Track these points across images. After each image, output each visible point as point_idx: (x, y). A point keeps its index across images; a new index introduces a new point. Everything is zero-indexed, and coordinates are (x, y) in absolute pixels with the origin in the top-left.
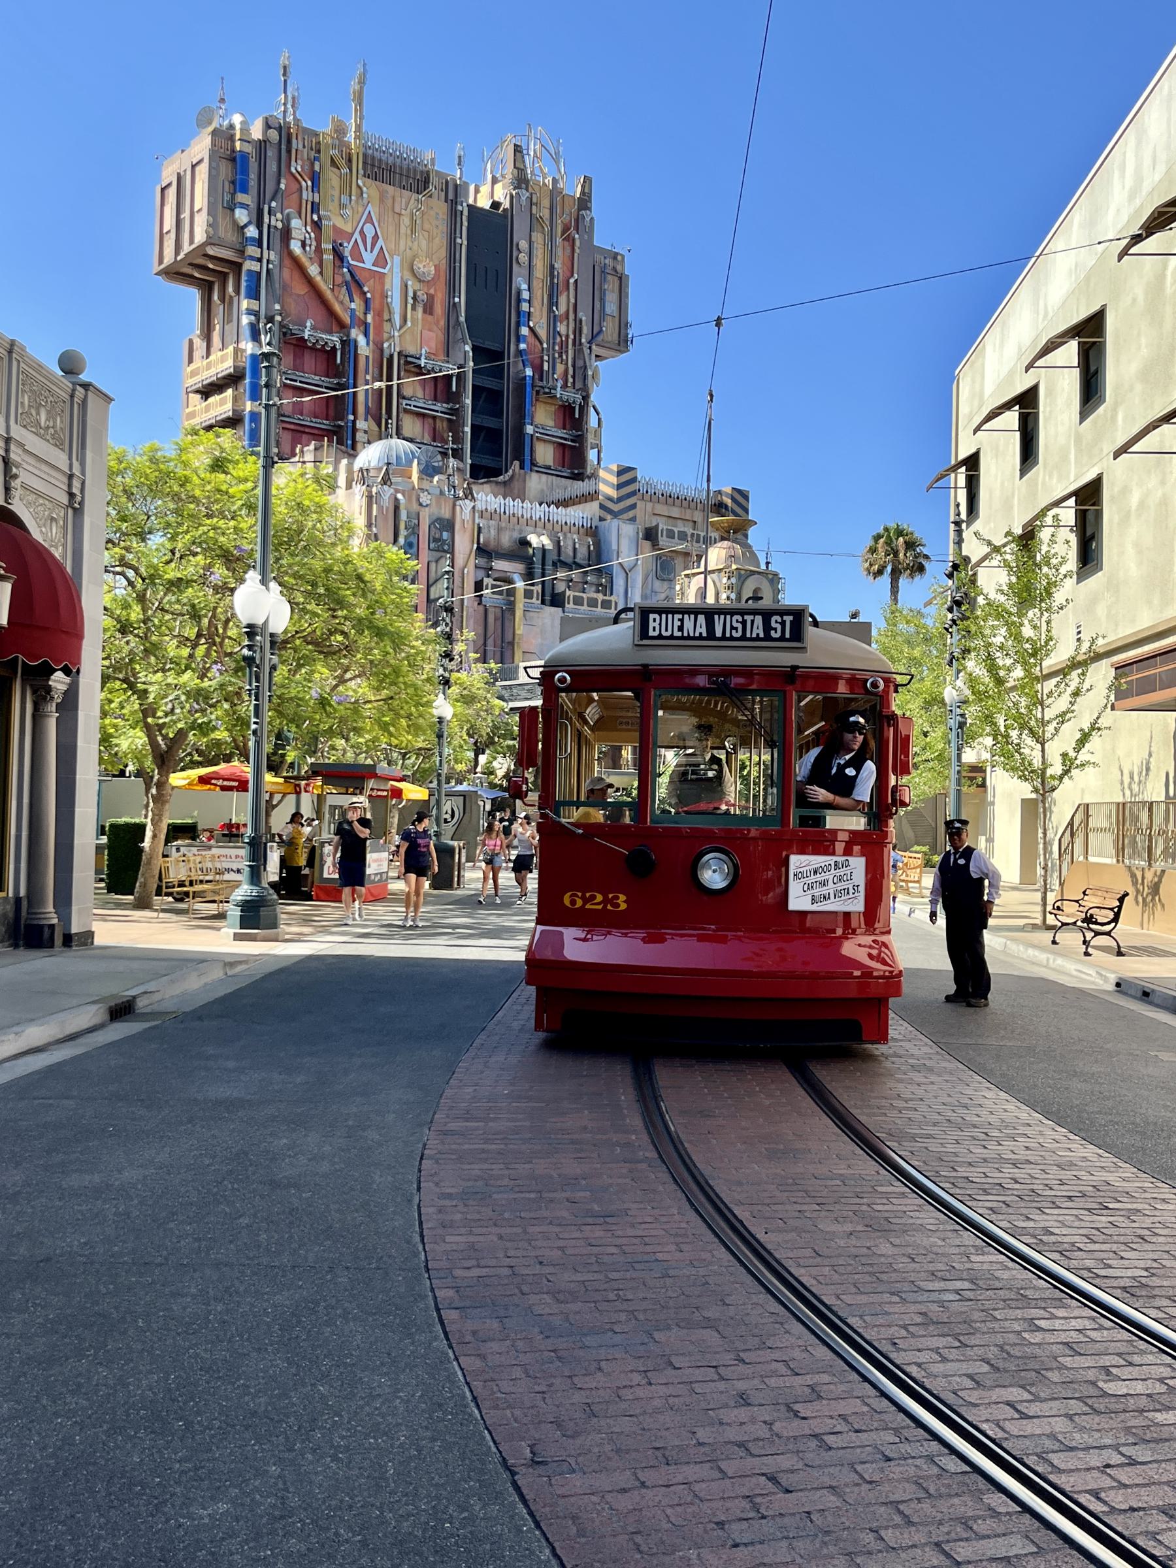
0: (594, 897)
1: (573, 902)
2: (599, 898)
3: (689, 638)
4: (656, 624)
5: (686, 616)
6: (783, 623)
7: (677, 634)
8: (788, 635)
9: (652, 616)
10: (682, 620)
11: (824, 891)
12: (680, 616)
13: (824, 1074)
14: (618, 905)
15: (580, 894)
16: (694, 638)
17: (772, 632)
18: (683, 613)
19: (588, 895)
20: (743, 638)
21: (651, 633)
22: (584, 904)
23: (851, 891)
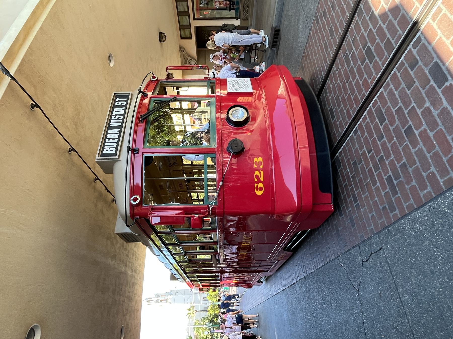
0: (257, 176)
1: (261, 189)
2: (257, 173)
3: (119, 136)
4: (109, 150)
5: (108, 137)
6: (119, 101)
7: (116, 141)
8: (126, 99)
12: (107, 140)
13: (279, 157)
14: (260, 162)
15: (256, 185)
16: (120, 134)
17: (123, 105)
18: (106, 139)
19: (256, 180)
20: (124, 115)
22: (261, 182)
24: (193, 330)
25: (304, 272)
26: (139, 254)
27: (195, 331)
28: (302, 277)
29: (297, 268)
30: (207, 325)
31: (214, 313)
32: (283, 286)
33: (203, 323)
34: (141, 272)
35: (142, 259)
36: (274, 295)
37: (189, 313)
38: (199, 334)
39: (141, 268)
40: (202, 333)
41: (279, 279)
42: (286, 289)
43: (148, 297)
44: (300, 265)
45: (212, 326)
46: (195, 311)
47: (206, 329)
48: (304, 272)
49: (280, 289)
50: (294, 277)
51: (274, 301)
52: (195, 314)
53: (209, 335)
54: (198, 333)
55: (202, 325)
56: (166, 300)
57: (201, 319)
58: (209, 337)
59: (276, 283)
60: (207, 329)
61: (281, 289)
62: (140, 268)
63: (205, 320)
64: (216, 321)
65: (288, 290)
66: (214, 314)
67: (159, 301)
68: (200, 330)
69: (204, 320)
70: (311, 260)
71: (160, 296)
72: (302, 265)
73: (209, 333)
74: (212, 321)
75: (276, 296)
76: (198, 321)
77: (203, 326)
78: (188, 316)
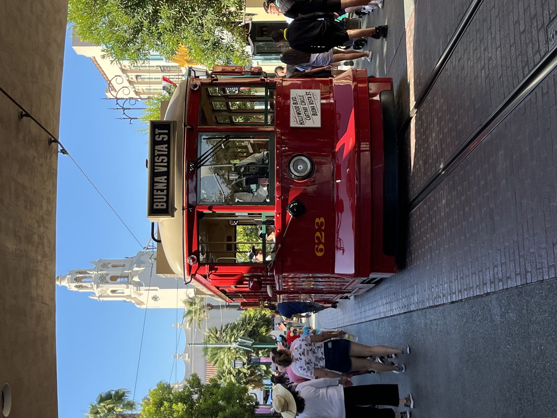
1: (321, 250)
6: (160, 134)
9: (155, 207)
10: (157, 190)
11: (309, 109)
15: (316, 246)
19: (317, 241)
21: (165, 207)
22: (322, 243)
23: (309, 96)
24: (203, 354)
25: (520, 274)
26: (35, 192)
27: (208, 357)
28: (511, 284)
29: (499, 257)
30: (241, 344)
31: (260, 313)
32: (455, 293)
33: (228, 338)
34: (45, 241)
35: (44, 203)
36: (427, 308)
37: (190, 312)
38: (218, 363)
39: (47, 228)
40: (226, 362)
41: (444, 270)
42: (461, 300)
43: (78, 269)
44: (511, 251)
45: (254, 346)
46: (209, 305)
47: (237, 352)
48: (520, 274)
49: (444, 296)
50: (488, 276)
51: (426, 325)
52: (206, 315)
53: (246, 368)
54: (217, 360)
55: (226, 343)
56: (127, 277)
57: (224, 328)
58: (245, 371)
59: (435, 280)
60: (241, 352)
61: (447, 298)
62: (42, 229)
63: (235, 331)
64: (264, 334)
65: (466, 305)
66: (259, 316)
67: (108, 278)
68: (222, 355)
69: (232, 331)
70: (545, 248)
71: (110, 266)
72: (516, 253)
73: (244, 364)
74: (254, 334)
75: (431, 310)
76: (217, 333)
77: (229, 346)
78: (189, 318)
